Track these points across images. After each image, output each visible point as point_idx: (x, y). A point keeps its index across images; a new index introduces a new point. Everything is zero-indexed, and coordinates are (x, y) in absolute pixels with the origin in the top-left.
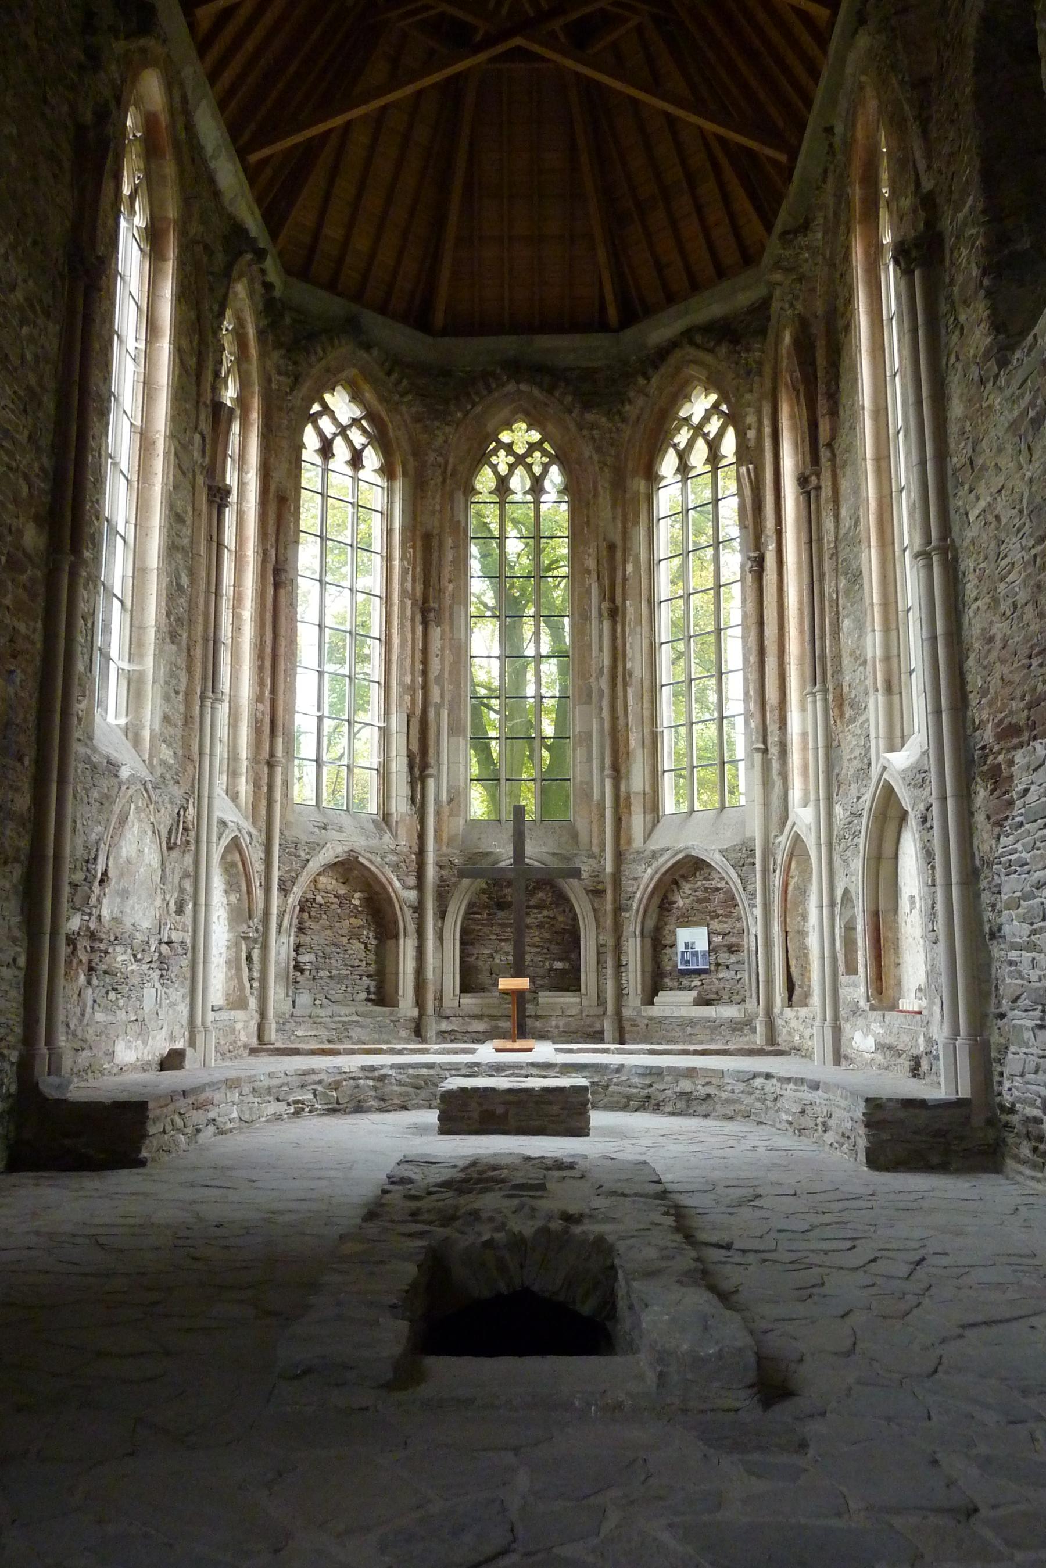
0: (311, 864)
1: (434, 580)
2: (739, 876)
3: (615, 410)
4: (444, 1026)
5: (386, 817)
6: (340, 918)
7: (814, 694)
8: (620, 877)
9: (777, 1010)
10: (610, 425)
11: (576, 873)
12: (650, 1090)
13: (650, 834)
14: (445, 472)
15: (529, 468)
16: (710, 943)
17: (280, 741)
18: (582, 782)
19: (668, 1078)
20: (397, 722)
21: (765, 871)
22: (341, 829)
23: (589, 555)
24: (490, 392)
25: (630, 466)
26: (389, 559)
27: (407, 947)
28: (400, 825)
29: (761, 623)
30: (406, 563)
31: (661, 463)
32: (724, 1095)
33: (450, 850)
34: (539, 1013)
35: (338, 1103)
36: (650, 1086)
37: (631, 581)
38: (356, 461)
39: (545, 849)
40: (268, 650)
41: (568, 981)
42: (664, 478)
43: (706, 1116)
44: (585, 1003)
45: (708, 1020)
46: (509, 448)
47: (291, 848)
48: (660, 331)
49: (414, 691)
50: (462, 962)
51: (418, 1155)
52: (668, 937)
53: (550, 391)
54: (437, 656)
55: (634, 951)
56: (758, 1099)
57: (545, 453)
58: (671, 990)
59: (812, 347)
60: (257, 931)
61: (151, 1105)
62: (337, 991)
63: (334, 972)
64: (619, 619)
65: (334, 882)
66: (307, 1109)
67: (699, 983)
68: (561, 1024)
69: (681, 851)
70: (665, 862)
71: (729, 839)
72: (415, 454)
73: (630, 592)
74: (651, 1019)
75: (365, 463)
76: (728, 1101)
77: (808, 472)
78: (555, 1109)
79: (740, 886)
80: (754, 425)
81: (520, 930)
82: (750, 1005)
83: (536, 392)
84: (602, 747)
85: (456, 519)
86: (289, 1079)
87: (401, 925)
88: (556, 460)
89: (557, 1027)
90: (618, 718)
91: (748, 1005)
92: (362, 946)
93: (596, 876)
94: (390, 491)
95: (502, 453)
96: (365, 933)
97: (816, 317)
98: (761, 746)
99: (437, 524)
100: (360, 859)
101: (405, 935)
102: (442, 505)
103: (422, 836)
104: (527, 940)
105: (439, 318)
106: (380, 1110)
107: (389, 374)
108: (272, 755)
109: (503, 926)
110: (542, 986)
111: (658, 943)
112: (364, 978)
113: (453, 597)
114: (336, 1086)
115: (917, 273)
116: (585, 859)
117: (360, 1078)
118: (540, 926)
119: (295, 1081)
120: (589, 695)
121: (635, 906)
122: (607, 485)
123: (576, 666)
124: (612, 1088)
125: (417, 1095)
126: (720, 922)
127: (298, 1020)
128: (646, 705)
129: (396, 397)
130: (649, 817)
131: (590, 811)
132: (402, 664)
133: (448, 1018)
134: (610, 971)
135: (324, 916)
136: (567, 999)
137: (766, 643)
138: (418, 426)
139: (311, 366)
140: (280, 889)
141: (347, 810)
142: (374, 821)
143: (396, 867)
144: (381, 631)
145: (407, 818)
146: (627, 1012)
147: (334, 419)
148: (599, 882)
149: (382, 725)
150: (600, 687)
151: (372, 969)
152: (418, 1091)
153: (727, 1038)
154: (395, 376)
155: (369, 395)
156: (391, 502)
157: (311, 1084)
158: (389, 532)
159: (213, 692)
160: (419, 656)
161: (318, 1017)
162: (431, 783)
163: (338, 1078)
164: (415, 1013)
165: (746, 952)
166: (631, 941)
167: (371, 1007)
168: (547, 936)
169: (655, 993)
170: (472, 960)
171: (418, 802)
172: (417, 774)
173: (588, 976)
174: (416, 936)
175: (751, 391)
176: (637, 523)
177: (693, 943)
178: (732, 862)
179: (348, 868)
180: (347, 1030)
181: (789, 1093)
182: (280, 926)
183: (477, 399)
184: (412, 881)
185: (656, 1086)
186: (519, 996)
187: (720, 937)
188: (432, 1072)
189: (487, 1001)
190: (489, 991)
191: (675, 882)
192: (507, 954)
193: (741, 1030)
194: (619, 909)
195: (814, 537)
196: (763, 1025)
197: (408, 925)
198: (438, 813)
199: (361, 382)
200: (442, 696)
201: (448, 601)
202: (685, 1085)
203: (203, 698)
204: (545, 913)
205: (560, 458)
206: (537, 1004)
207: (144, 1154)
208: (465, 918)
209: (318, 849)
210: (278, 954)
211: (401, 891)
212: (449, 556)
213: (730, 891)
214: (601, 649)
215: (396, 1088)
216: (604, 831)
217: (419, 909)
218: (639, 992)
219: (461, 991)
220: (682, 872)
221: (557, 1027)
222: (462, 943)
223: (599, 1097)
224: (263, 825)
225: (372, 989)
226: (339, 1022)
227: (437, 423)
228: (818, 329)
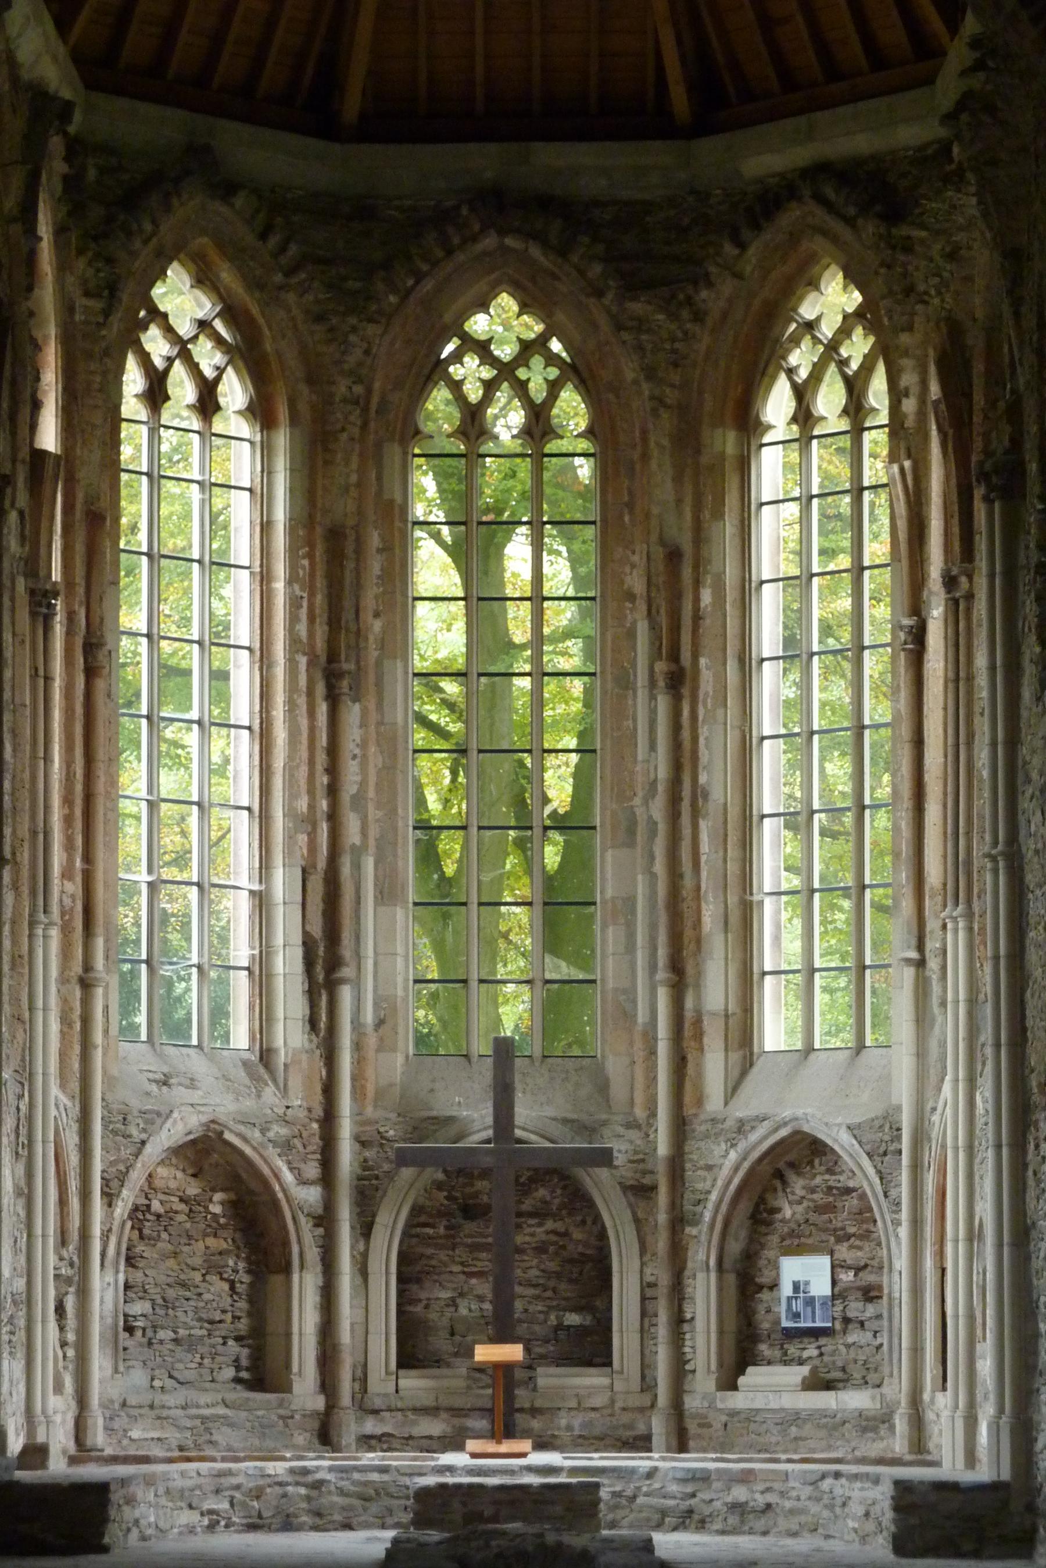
0: (148, 1149)
1: (348, 615)
2: (879, 1172)
3: (681, 297)
4: (371, 1426)
5: (266, 1055)
6: (190, 1237)
7: (955, 919)
8: (683, 1162)
9: (926, 1396)
10: (673, 327)
11: (604, 1158)
12: (693, 1501)
13: (735, 1089)
14: (366, 410)
15: (521, 388)
16: (834, 1282)
17: (100, 943)
18: (616, 990)
19: (717, 1485)
20: (283, 883)
21: (916, 1167)
22: (192, 1084)
23: (633, 566)
24: (450, 252)
25: (709, 403)
26: (265, 578)
27: (305, 1287)
28: (291, 1069)
29: (918, 742)
30: (296, 587)
31: (765, 399)
32: (788, 1504)
33: (380, 1114)
34: (538, 1404)
35: (260, 1516)
36: (693, 1495)
37: (708, 621)
38: (207, 404)
39: (550, 1112)
40: (79, 788)
41: (591, 1348)
42: (770, 427)
43: (765, 1533)
44: (618, 1386)
45: (824, 1413)
46: (483, 348)
47: (119, 1123)
48: (768, 156)
49: (314, 825)
50: (400, 1312)
51: (909, 932)
52: (766, 1272)
53: (563, 252)
54: (354, 757)
55: (704, 1295)
56: (826, 1506)
57: (552, 359)
58: (769, 1363)
59: (967, 365)
60: (72, 1265)
61: (112, 1488)
62: (187, 1367)
63: (182, 1332)
64: (686, 691)
65: (180, 1175)
66: (223, 1523)
67: (816, 1352)
68: (576, 1423)
69: (785, 1124)
70: (760, 1140)
71: (864, 1107)
72: (311, 381)
73: (708, 641)
74: (733, 1413)
75: (222, 401)
76: (792, 1512)
77: (955, 571)
78: (558, 1510)
79: (879, 1189)
80: (915, 390)
81: (505, 1258)
82: (888, 1390)
83: (535, 252)
84: (653, 927)
85: (386, 497)
86: (202, 1480)
87: (295, 1249)
88: (572, 375)
89: (569, 1428)
90: (681, 876)
91: (885, 1389)
92: (226, 1286)
93: (641, 1160)
94: (267, 450)
95: (471, 361)
96: (231, 1263)
97: (975, 320)
98: (914, 955)
99: (351, 507)
100: (228, 1136)
101: (302, 1267)
102: (362, 471)
103: (329, 1090)
104: (518, 1272)
105: (352, 105)
106: (316, 1528)
107: (263, 236)
108: (88, 967)
109: (475, 1248)
110: (542, 1357)
111: (747, 1282)
112: (231, 1342)
113: (382, 646)
114: (258, 1494)
115: (997, 506)
116: (621, 1130)
117: (287, 1484)
118: (541, 1249)
119: (209, 1484)
120: (631, 831)
121: (707, 1216)
122: (665, 442)
123: (608, 771)
124: (641, 1500)
125: (365, 1509)
126: (851, 1247)
127: (135, 1412)
128: (733, 852)
129: (278, 278)
130: (735, 1056)
131: (631, 1044)
132: (292, 776)
133: (376, 1412)
134: (662, 1331)
135: (164, 1236)
136: (589, 1381)
137: (927, 777)
138: (317, 328)
139: (133, 254)
140: (104, 1193)
141: (199, 1047)
142: (245, 1064)
143: (286, 1147)
144: (251, 713)
145: (304, 1057)
146: (692, 1403)
147: (169, 331)
148: (644, 1173)
149: (256, 887)
150: (650, 817)
151: (243, 1326)
152: (368, 1504)
153: (853, 1444)
154: (273, 241)
155: (227, 276)
156: (267, 471)
157: (227, 1489)
158: (266, 527)
159: (45, 912)
160: (321, 758)
161: (163, 1407)
162: (346, 995)
163: (261, 1482)
164: (319, 1403)
165: (885, 1298)
166: (701, 1276)
167: (242, 1394)
168: (552, 1266)
169: (741, 1370)
170: (418, 1309)
171: (322, 1025)
172: (321, 978)
173: (624, 1340)
174: (319, 1268)
175: (910, 328)
176: (718, 514)
177: (807, 1283)
178: (868, 1147)
179: (207, 1154)
180: (207, 1430)
181: (856, 1494)
182: (103, 1255)
183: (425, 267)
184: (313, 1170)
185: (700, 1495)
186: (505, 1369)
187: (851, 1274)
188: (386, 1477)
189: (446, 1383)
190: (448, 1365)
191: (779, 1175)
192: (481, 1299)
193: (875, 1429)
194: (679, 1221)
195: (962, 674)
196: (906, 1419)
197: (306, 1249)
198: (358, 1046)
199: (213, 255)
200: (364, 833)
201: (372, 654)
202: (740, 1493)
203: (32, 924)
204: (550, 1225)
205: (577, 372)
206: (535, 1389)
207: (106, 1540)
208: (407, 1234)
209: (159, 1121)
210: (102, 1302)
211: (297, 1190)
212: (375, 566)
213: (863, 1197)
214: (652, 747)
215: (336, 1499)
216: (655, 1078)
217: (325, 1220)
218: (713, 1367)
219: (400, 1365)
220: (791, 1157)
221: (569, 1428)
222: (401, 1279)
223: (620, 1514)
224: (75, 1086)
225: (244, 1362)
226: (197, 1417)
227: (353, 320)
228: (975, 340)
